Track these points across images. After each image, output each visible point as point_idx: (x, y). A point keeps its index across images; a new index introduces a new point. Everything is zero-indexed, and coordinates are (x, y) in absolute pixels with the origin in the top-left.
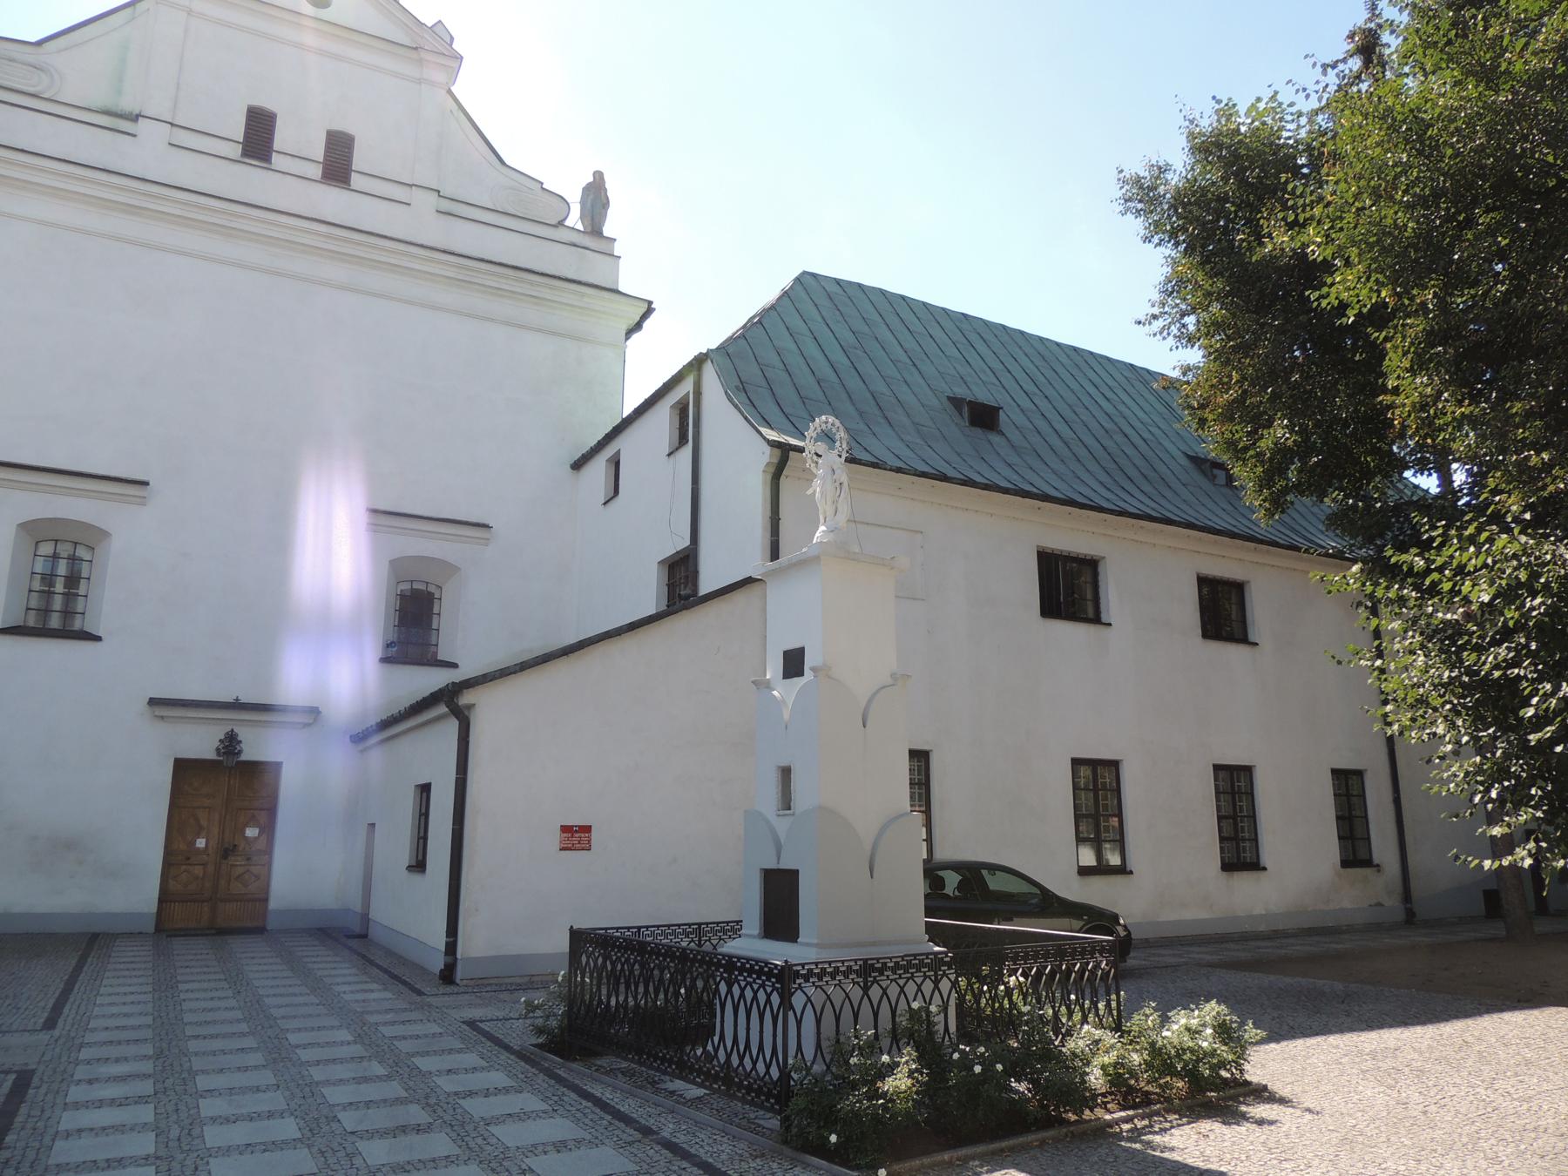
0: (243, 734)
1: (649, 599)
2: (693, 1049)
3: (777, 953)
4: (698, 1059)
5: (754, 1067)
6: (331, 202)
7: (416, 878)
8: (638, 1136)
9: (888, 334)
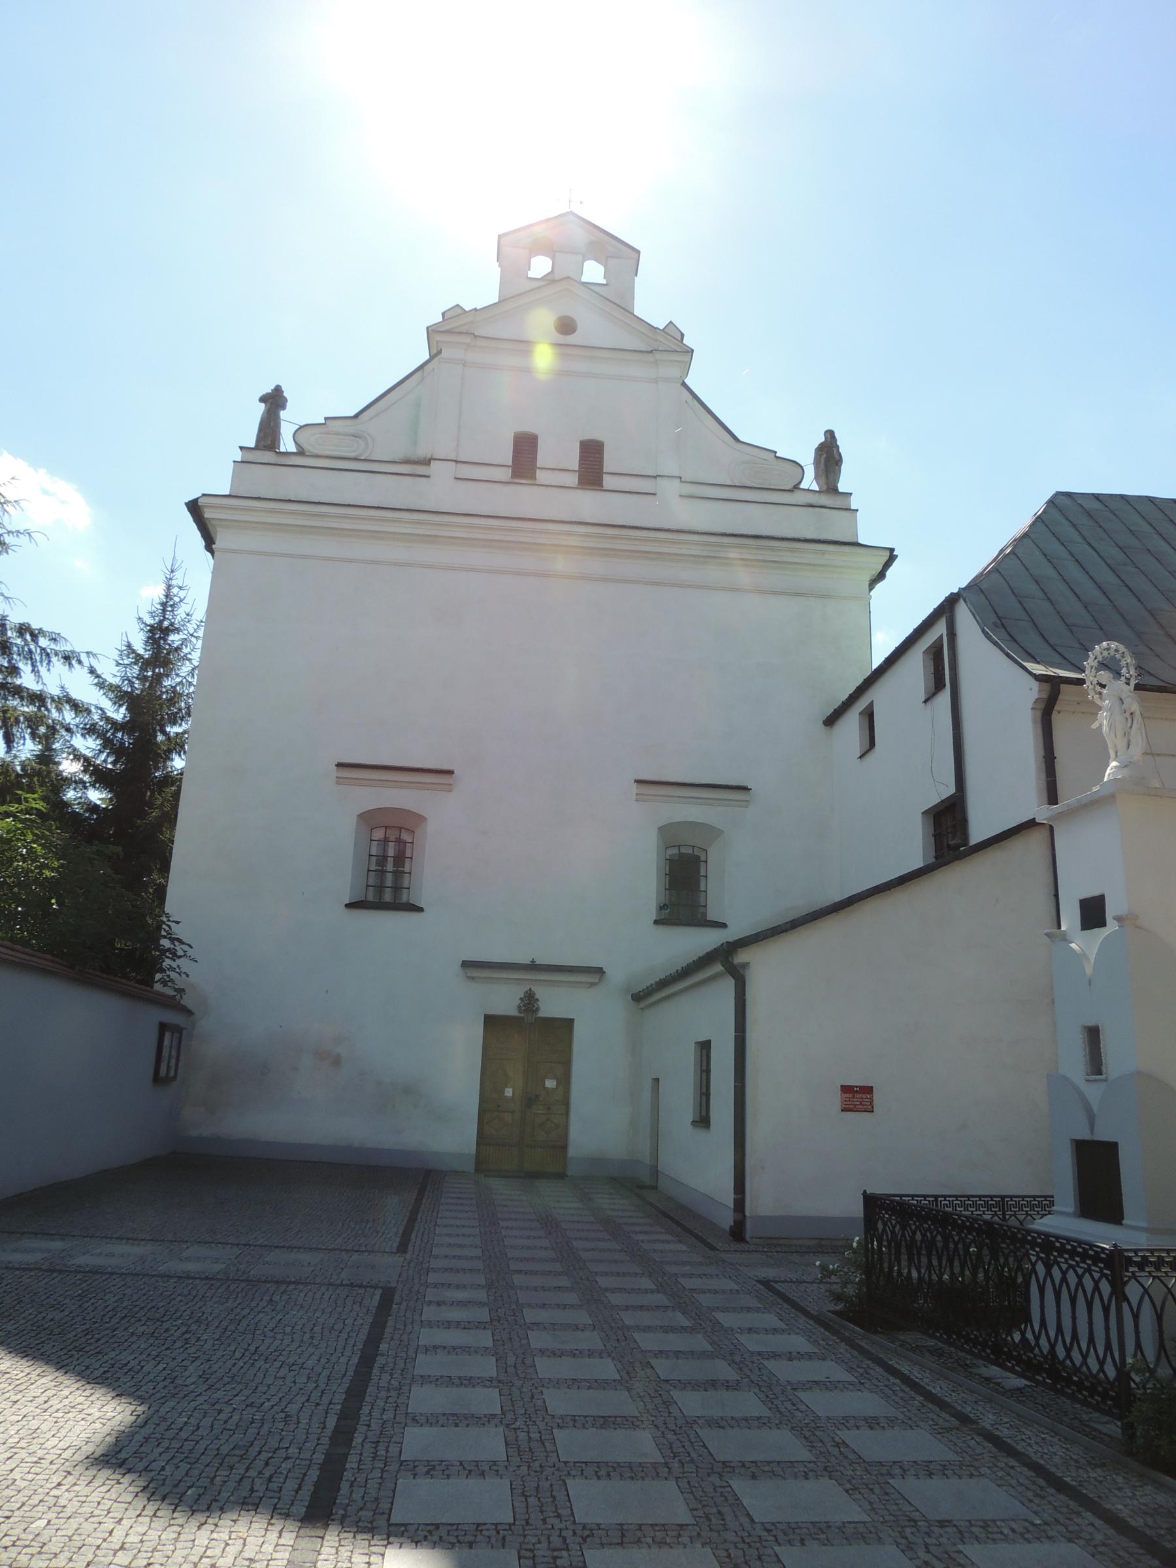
0: (540, 992)
1: (913, 851)
2: (1010, 1333)
3: (1103, 1236)
4: (1016, 1345)
5: (1084, 1362)
6: (589, 504)
7: (701, 1134)
8: (955, 1422)
9: (1163, 543)
